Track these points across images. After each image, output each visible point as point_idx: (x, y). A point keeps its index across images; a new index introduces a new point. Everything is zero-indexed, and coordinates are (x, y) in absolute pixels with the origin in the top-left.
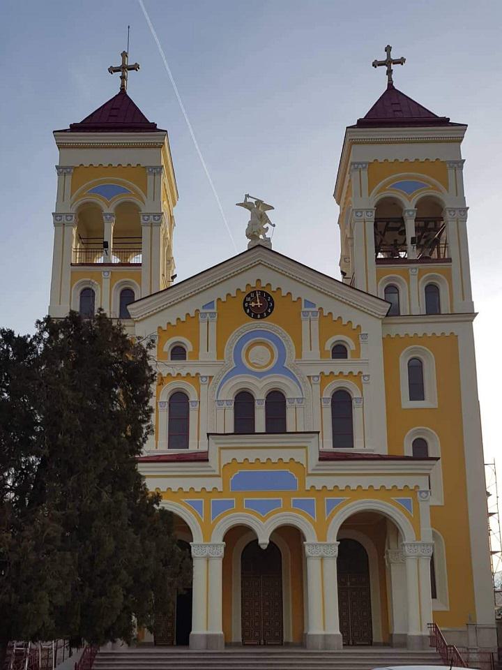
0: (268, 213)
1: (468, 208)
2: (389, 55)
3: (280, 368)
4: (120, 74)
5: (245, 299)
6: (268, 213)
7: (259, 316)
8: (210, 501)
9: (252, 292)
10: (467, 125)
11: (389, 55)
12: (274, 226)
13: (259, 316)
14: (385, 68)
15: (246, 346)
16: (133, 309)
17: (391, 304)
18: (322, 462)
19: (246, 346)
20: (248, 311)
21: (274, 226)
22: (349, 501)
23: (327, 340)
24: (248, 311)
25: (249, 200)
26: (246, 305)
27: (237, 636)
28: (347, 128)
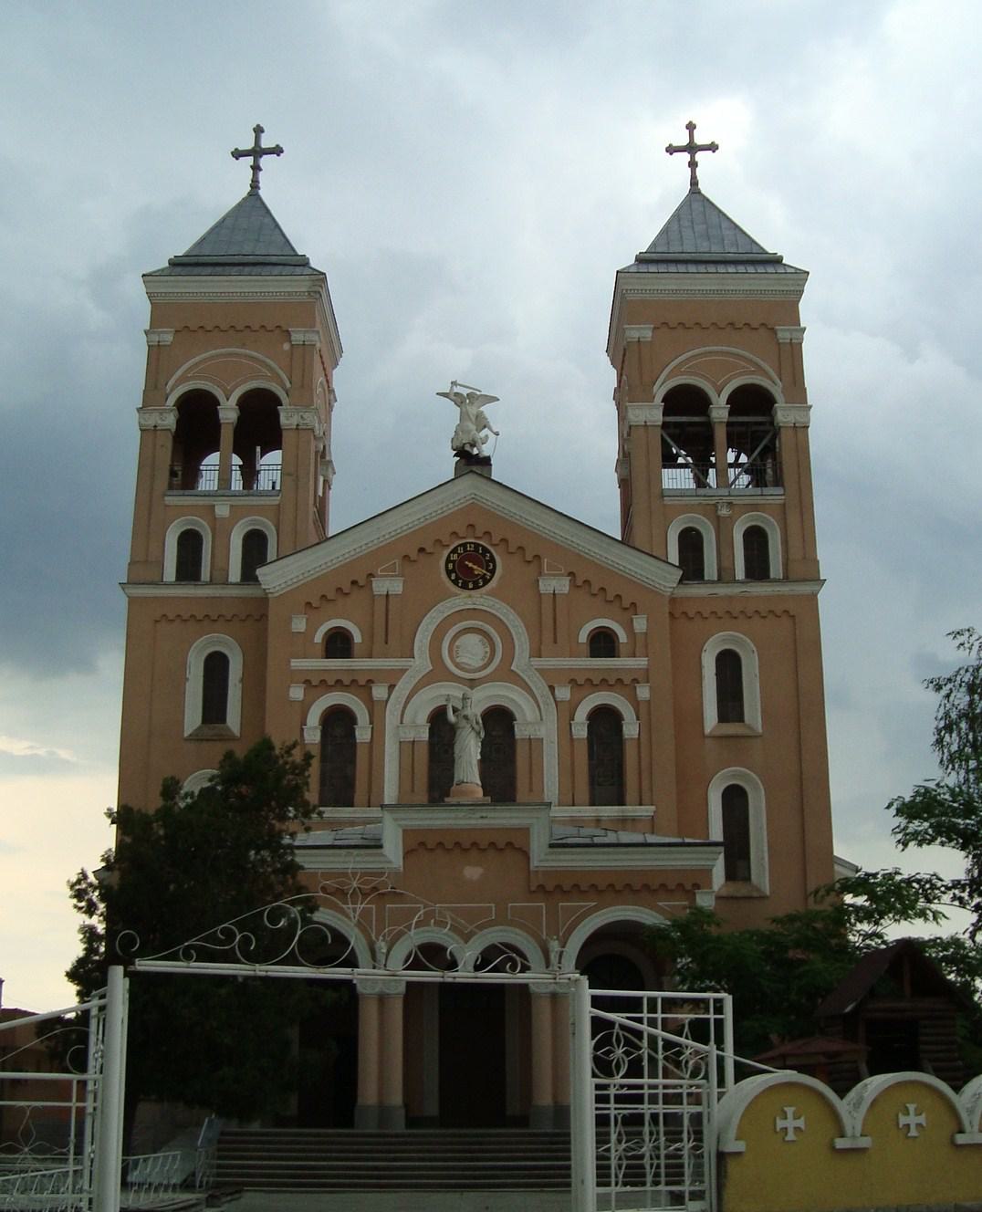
0: (487, 409)
1: (811, 407)
2: (693, 157)
3: (506, 674)
4: (250, 160)
5: (449, 556)
6: (487, 409)
7: (471, 586)
8: (385, 907)
9: (460, 545)
10: (808, 273)
11: (693, 157)
12: (497, 434)
13: (471, 586)
14: (686, 157)
15: (451, 633)
16: (265, 575)
17: (908, 1138)
18: (551, 850)
19: (451, 633)
20: (453, 577)
21: (497, 434)
22: (596, 909)
23: (360, 630)
24: (453, 577)
25: (457, 389)
26: (451, 566)
27: (432, 1107)
28: (618, 272)
